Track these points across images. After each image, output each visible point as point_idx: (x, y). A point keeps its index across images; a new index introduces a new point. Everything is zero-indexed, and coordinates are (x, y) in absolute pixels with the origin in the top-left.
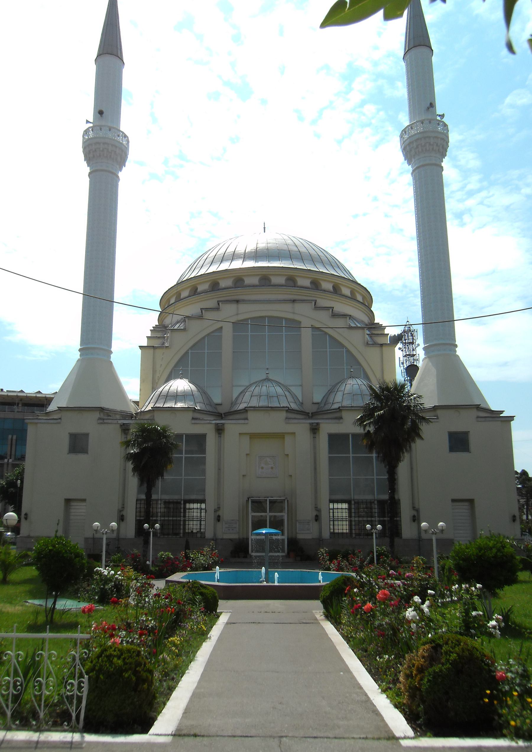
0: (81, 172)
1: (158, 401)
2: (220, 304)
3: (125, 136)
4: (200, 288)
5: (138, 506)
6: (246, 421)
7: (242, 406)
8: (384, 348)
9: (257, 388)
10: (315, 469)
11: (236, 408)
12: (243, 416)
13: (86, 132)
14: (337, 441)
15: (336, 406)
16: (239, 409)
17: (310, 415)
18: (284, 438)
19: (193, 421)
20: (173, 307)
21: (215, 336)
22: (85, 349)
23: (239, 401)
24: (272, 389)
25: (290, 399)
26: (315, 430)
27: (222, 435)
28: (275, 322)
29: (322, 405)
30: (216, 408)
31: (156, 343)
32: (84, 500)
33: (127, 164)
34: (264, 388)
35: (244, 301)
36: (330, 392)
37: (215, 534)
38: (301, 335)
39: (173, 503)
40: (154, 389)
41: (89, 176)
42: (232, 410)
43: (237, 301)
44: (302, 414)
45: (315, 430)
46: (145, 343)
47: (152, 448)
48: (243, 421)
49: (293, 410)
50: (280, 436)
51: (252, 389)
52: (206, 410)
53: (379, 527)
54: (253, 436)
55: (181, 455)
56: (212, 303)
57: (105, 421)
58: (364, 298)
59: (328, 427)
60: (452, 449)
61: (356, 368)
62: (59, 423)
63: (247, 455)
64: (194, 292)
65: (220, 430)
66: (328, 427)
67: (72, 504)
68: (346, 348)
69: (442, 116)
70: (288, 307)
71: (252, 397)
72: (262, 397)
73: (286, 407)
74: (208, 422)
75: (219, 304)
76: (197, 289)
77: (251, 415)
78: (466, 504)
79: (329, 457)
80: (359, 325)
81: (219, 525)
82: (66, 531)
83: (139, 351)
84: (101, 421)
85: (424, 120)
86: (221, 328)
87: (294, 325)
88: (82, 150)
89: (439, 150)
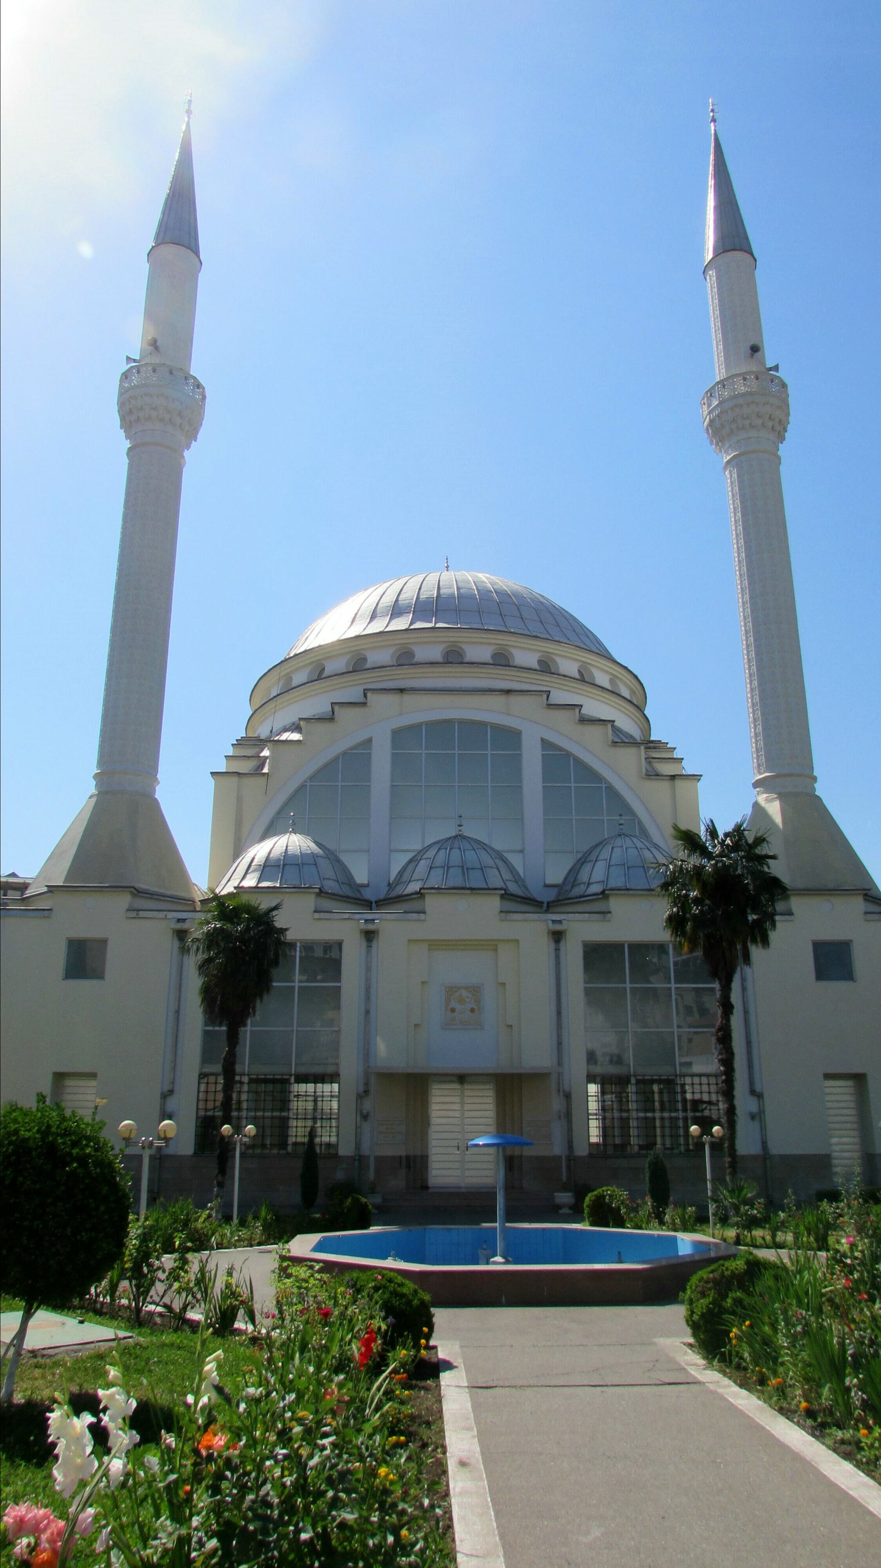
0: (112, 450)
1: (248, 876)
2: (369, 695)
3: (199, 386)
4: (329, 669)
5: (203, 1087)
6: (422, 916)
7: (414, 887)
8: (678, 783)
9: (442, 852)
10: (559, 1013)
11: (399, 891)
12: (415, 905)
13: (126, 376)
14: (600, 957)
15: (596, 888)
16: (406, 892)
17: (545, 905)
18: (496, 950)
19: (317, 915)
20: (273, 705)
21: (357, 758)
22: (108, 776)
23: (405, 877)
24: (470, 856)
25: (507, 875)
26: (557, 936)
27: (374, 944)
28: (473, 730)
29: (568, 887)
30: (359, 891)
31: (245, 767)
32: (93, 1076)
33: (199, 436)
34: (456, 853)
35: (413, 690)
36: (582, 861)
37: (358, 1147)
38: (520, 755)
39: (274, 1081)
40: (238, 852)
41: (128, 454)
42: (392, 895)
43: (402, 691)
44: (529, 904)
45: (557, 936)
46: (222, 766)
47: (243, 955)
48: (415, 916)
49: (512, 895)
50: (492, 946)
51: (431, 853)
52: (341, 893)
53: (718, 1131)
54: (434, 945)
55: (294, 979)
56: (353, 693)
57: (142, 914)
58: (632, 692)
59: (583, 929)
60: (822, 974)
61: (627, 823)
62: (48, 917)
63: (423, 983)
64: (319, 675)
65: (370, 936)
66: (583, 929)
67: (69, 1082)
68: (607, 782)
69: (776, 369)
70: (499, 701)
71: (432, 871)
72: (451, 870)
73: (501, 889)
74: (347, 916)
75: (365, 696)
76: (324, 669)
77: (431, 902)
78: (850, 1083)
79: (586, 988)
80: (627, 741)
81: (366, 1127)
82: (764, 1144)
83: (211, 782)
84: (134, 912)
85: (747, 373)
86: (370, 740)
87: (509, 738)
88: (116, 408)
89: (773, 427)
